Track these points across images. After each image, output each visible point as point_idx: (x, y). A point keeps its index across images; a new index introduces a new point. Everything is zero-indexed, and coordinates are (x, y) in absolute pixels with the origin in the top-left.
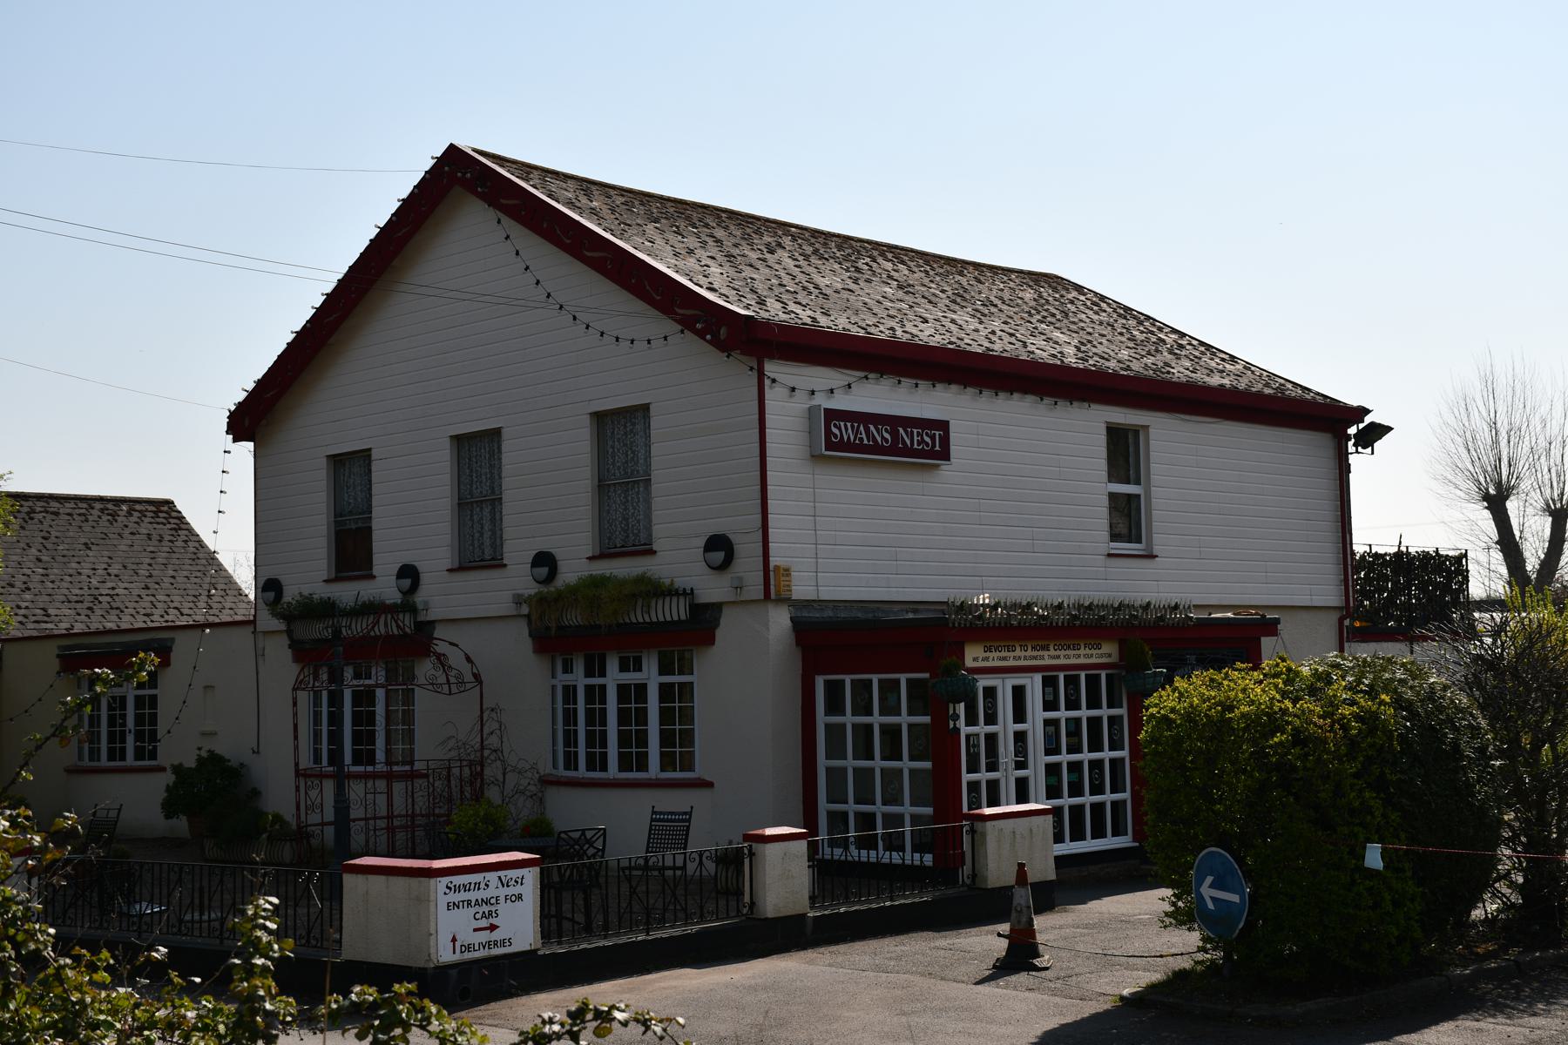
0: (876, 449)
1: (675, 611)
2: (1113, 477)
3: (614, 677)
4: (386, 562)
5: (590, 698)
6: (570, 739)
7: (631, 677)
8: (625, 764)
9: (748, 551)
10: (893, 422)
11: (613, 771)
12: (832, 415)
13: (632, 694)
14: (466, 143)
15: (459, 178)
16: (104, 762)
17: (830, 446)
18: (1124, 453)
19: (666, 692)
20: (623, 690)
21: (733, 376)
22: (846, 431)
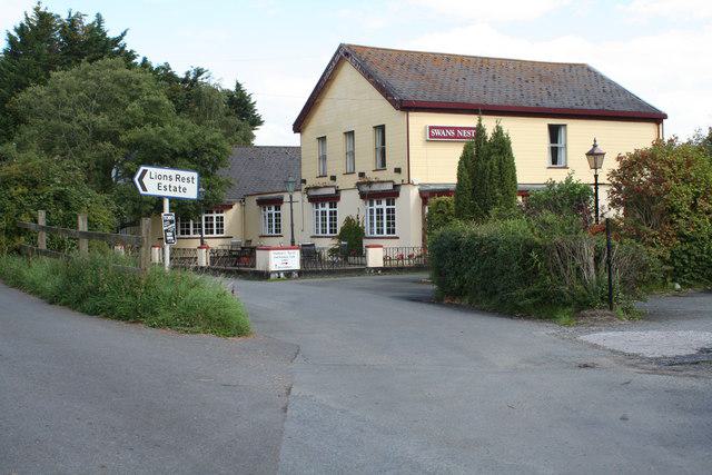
0: (449, 137)
1: (389, 187)
2: (552, 142)
3: (375, 206)
4: (391, 163)
5: (378, 212)
6: (324, 225)
7: (379, 207)
8: (388, 232)
9: (404, 170)
10: (456, 129)
11: (385, 234)
12: (431, 128)
13: (380, 211)
14: (347, 42)
15: (344, 55)
16: (274, 233)
17: (431, 137)
18: (554, 132)
19: (388, 211)
20: (378, 210)
21: (402, 115)
22: (438, 133)
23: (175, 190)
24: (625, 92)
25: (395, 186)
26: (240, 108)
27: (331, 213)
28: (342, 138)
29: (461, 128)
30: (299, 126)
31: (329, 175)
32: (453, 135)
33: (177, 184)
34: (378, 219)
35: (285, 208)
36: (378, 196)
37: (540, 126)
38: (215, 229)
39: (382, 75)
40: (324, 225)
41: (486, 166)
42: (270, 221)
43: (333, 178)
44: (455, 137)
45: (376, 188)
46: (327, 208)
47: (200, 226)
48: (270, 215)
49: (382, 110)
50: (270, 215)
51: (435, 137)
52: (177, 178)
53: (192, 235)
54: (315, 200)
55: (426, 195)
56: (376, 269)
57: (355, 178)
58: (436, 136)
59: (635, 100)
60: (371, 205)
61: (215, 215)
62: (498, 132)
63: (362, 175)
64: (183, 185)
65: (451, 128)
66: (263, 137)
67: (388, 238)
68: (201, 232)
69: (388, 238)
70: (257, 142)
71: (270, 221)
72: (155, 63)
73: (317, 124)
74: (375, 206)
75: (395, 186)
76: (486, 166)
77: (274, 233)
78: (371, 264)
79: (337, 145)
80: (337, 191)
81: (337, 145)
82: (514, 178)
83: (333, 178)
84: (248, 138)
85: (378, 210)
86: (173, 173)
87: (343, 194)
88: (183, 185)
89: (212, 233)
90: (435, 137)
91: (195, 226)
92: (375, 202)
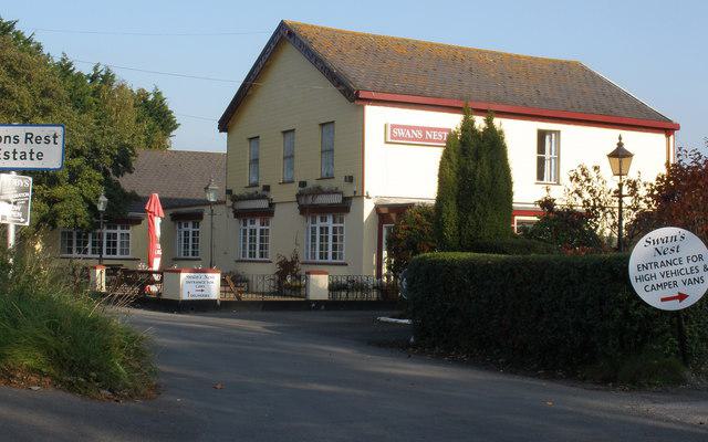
1: (336, 199)
2: (539, 153)
3: (319, 224)
6: (252, 247)
7: (323, 224)
10: (424, 129)
12: (393, 127)
13: (253, 232)
15: (285, 36)
22: (401, 133)
23: (23, 157)
24: (627, 96)
25: (345, 199)
26: (157, 116)
27: (262, 231)
28: (280, 138)
29: (430, 129)
30: (225, 124)
31: (262, 184)
32: (422, 137)
33: (27, 148)
34: (321, 240)
35: (205, 224)
36: (324, 210)
37: (533, 127)
38: (118, 248)
39: (331, 57)
40: (252, 247)
41: (475, 168)
42: (186, 241)
43: (267, 188)
44: (423, 139)
45: (323, 200)
46: (258, 226)
47: (101, 245)
48: (186, 233)
49: (327, 100)
50: (186, 233)
51: (398, 138)
52: (29, 138)
53: (89, 255)
54: (241, 215)
55: (391, 214)
56: (319, 303)
57: (295, 188)
58: (396, 136)
59: (641, 107)
60: (245, 225)
61: (119, 231)
62: (490, 128)
63: (303, 184)
64: (37, 148)
65: (415, 128)
66: (179, 141)
67: (320, 264)
68: (101, 252)
69: (320, 264)
70: (174, 147)
71: (186, 241)
72: (83, 67)
73: (248, 122)
74: (319, 224)
75: (345, 199)
76: (475, 168)
77: (190, 256)
78: (313, 295)
79: (272, 150)
80: (271, 205)
81: (272, 150)
82: (509, 194)
83: (267, 188)
84: (162, 146)
85: (122, 234)
86: (20, 131)
87: (277, 209)
88: (37, 148)
89: (114, 253)
90: (398, 138)
91: (94, 244)
92: (248, 221)
